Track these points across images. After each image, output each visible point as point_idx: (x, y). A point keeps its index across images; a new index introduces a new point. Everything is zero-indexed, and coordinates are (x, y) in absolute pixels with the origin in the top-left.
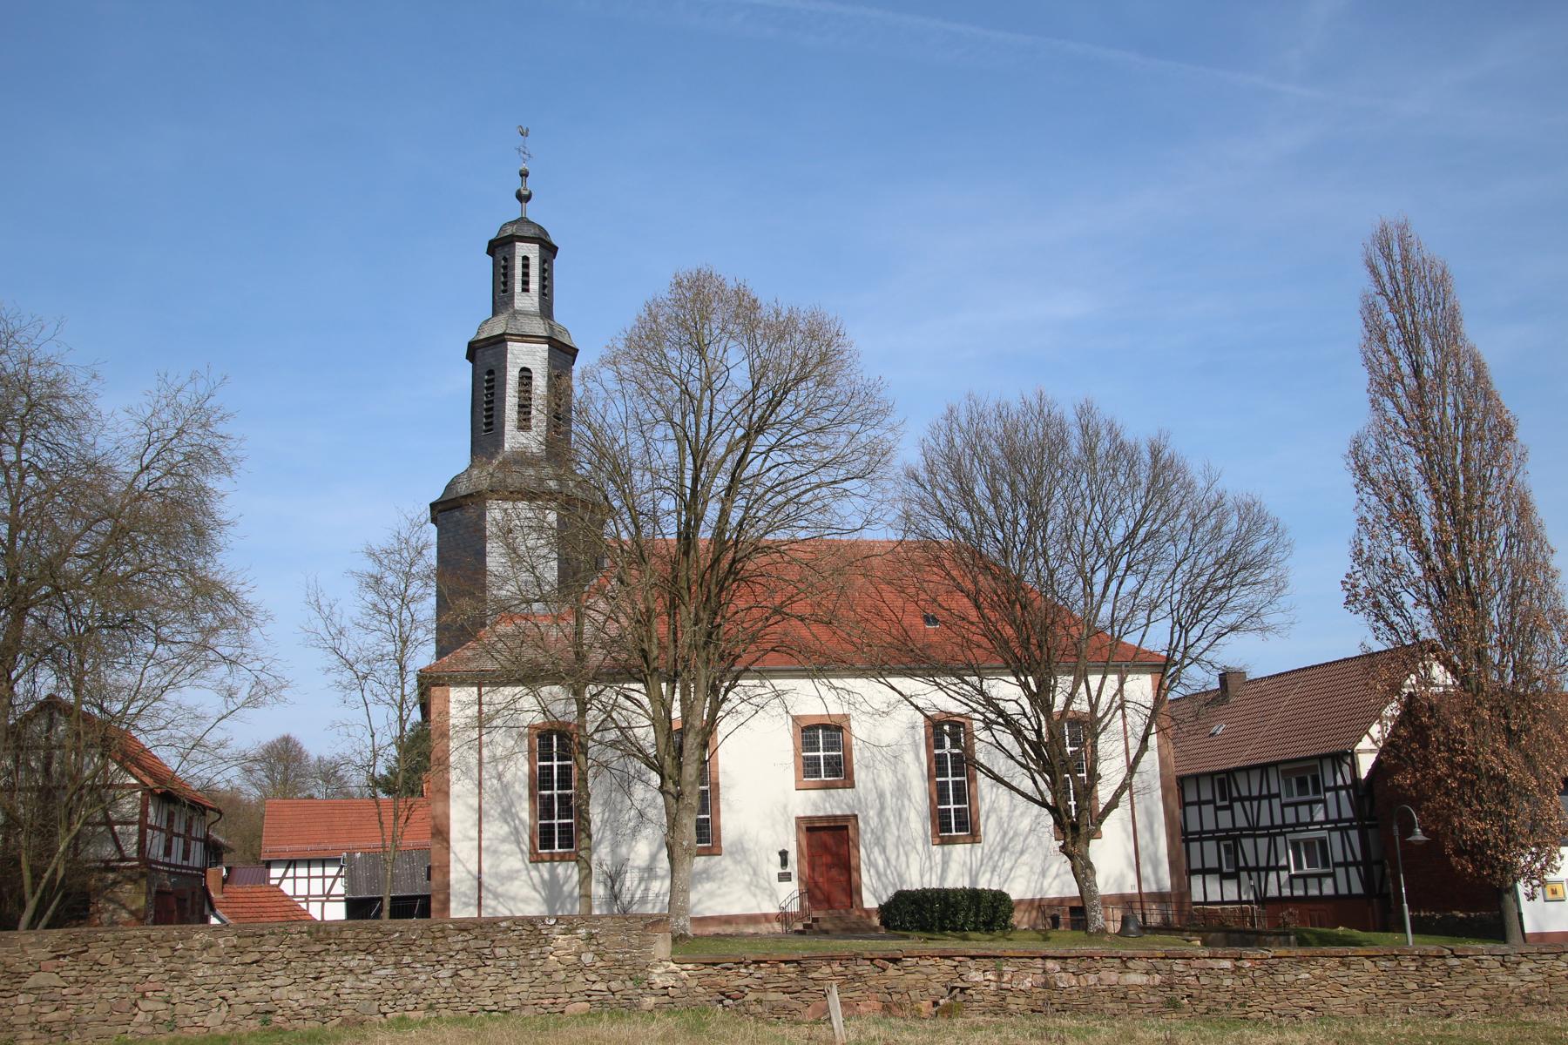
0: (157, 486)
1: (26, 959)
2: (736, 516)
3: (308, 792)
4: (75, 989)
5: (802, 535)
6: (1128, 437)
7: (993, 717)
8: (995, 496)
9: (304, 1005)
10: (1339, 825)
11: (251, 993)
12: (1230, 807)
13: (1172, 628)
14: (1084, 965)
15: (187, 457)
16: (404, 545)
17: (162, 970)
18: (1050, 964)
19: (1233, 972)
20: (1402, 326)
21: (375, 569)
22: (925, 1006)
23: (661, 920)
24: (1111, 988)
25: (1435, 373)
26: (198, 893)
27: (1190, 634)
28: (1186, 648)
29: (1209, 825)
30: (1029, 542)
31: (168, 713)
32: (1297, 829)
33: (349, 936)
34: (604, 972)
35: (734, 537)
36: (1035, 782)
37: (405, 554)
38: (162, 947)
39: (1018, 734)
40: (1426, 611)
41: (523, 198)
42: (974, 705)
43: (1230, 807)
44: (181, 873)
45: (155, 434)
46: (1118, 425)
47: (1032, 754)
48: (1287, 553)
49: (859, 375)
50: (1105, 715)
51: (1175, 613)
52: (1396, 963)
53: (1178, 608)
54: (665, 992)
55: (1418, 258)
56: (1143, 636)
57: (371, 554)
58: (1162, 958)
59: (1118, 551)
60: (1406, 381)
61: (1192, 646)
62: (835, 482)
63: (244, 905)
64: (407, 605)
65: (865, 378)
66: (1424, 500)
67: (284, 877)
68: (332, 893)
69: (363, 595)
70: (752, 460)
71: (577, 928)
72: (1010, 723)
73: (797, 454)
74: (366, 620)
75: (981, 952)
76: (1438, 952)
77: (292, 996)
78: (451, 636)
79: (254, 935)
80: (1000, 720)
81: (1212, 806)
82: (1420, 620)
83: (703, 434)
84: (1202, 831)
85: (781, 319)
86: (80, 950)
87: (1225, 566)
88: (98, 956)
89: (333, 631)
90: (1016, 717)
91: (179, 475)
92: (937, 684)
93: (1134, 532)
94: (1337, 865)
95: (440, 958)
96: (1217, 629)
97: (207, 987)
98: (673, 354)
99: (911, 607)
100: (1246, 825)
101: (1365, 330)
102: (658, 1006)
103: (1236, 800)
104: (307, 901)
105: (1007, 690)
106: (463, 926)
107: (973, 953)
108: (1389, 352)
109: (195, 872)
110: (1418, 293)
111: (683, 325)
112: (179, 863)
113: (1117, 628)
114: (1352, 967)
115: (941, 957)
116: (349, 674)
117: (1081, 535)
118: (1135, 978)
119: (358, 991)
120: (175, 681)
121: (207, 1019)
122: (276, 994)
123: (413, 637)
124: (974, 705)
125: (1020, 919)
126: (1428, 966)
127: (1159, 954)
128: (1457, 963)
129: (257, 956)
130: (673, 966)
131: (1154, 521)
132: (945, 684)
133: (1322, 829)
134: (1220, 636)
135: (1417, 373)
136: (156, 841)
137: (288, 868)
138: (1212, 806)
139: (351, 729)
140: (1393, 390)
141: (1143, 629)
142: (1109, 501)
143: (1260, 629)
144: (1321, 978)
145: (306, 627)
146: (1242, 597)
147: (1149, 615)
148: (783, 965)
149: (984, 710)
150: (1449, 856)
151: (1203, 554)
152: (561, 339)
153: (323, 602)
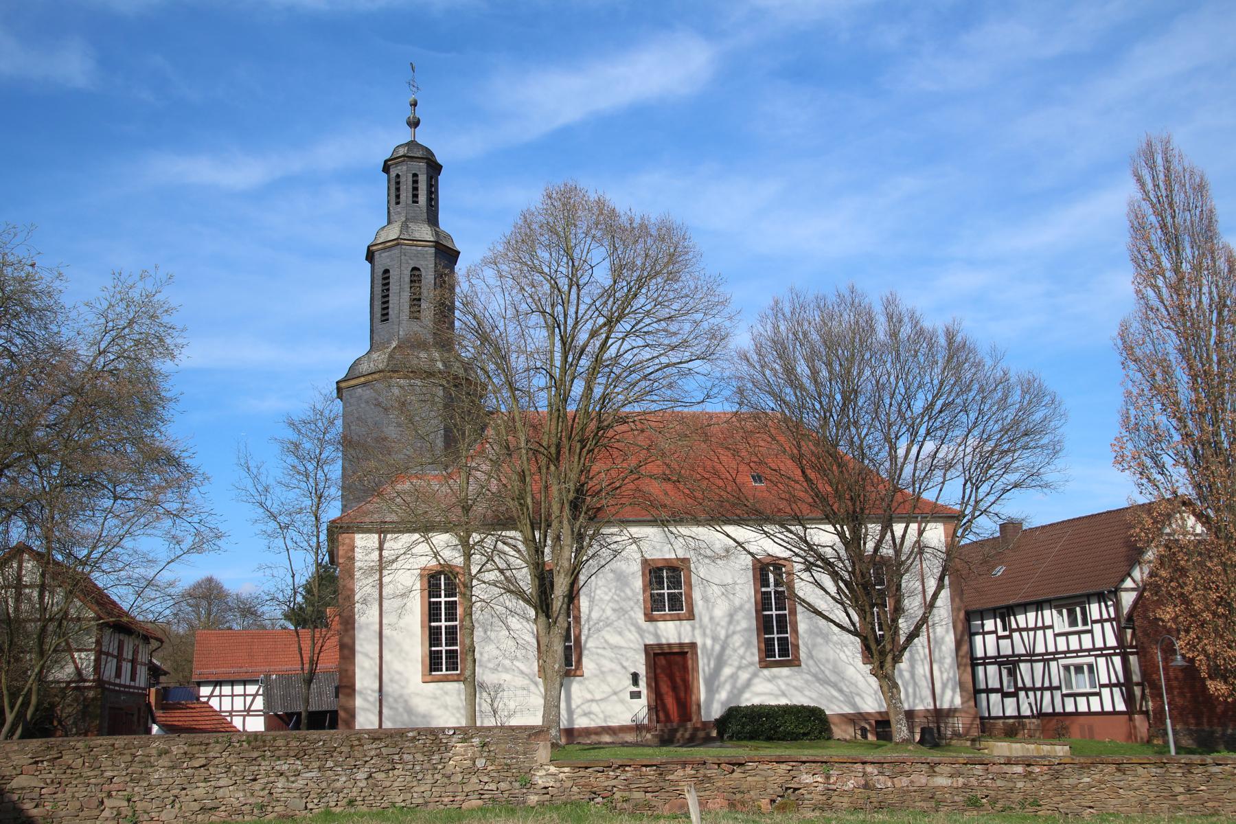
0: (111, 367)
1: (10, 764)
2: (598, 391)
3: (228, 624)
4: (51, 789)
5: (654, 407)
6: (927, 324)
7: (811, 559)
8: (815, 373)
9: (244, 802)
10: (1104, 652)
11: (200, 792)
12: (1010, 637)
13: (965, 485)
14: (897, 769)
15: (137, 343)
16: (318, 416)
17: (124, 773)
18: (869, 769)
19: (1025, 776)
20: (1163, 227)
21: (294, 437)
22: (764, 803)
23: (543, 731)
24: (921, 790)
25: (1193, 268)
26: (143, 708)
27: (980, 490)
28: (977, 502)
29: (992, 652)
30: (844, 409)
31: (126, 557)
32: (1068, 655)
33: (281, 744)
34: (495, 774)
35: (597, 409)
36: (848, 615)
37: (320, 424)
38: (124, 754)
39: (835, 576)
40: (1183, 471)
41: (414, 123)
42: (796, 550)
43: (1010, 637)
44: (129, 692)
45: (111, 324)
46: (918, 314)
47: (846, 591)
48: (1063, 421)
49: (702, 272)
50: (908, 558)
51: (967, 473)
52: (1164, 769)
53: (970, 469)
54: (544, 791)
55: (1179, 168)
56: (941, 490)
57: (292, 424)
58: (963, 764)
59: (918, 420)
60: (1168, 274)
61: (981, 500)
62: (681, 363)
63: (180, 719)
64: (322, 467)
65: (708, 275)
66: (1181, 376)
67: (211, 696)
68: (252, 708)
69: (284, 458)
70: (612, 345)
71: (472, 738)
72: (828, 566)
73: (650, 339)
74: (287, 480)
75: (811, 758)
76: (1202, 760)
77: (234, 796)
78: (353, 491)
79: (201, 744)
80: (819, 563)
81: (995, 635)
82: (1178, 478)
83: (570, 322)
84: (986, 657)
85: (634, 225)
86: (56, 756)
87: (1009, 433)
88: (70, 762)
89: (260, 489)
90: (831, 560)
91: (131, 358)
92: (765, 533)
93: (932, 404)
94: (1102, 686)
95: (357, 763)
96: (1003, 486)
97: (163, 787)
98: (544, 255)
99: (743, 468)
100: (1024, 652)
101: (1131, 230)
102: (541, 804)
103: (1015, 630)
104: (231, 716)
105: (825, 536)
106: (377, 736)
107: (804, 759)
108: (1151, 250)
109: (140, 691)
110: (1179, 198)
111: (553, 231)
112: (128, 683)
113: (917, 486)
114: (1127, 772)
115: (777, 762)
116: (273, 525)
117: (887, 406)
118: (941, 781)
119: (289, 790)
120: (131, 530)
121: (162, 814)
122: (220, 793)
123: (327, 494)
124: (796, 550)
125: (839, 732)
126: (1193, 773)
127: (961, 760)
128: (1218, 771)
129: (203, 762)
130: (553, 769)
131: (950, 393)
132: (772, 532)
133: (1089, 655)
134: (1005, 491)
135: (1177, 270)
136: (109, 665)
137: (215, 686)
138: (995, 635)
139: (275, 571)
140: (1156, 282)
141: (940, 486)
142: (910, 378)
143: (1040, 486)
144: (1101, 782)
145: (237, 485)
146: (1024, 460)
147: (945, 475)
148: (644, 769)
149: (804, 554)
150: (1205, 678)
151: (991, 422)
152: (445, 243)
153: (252, 464)
